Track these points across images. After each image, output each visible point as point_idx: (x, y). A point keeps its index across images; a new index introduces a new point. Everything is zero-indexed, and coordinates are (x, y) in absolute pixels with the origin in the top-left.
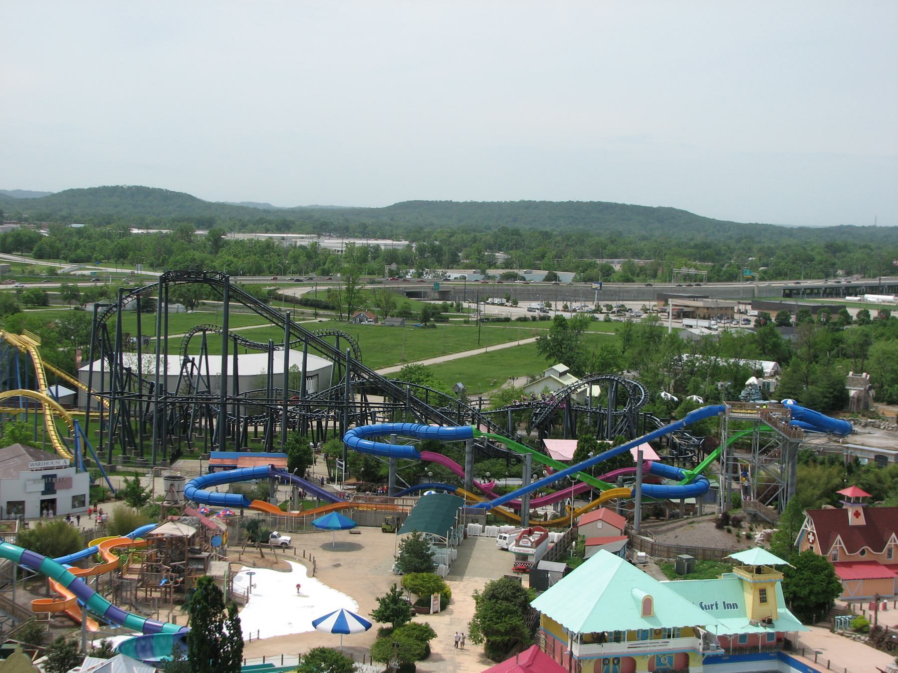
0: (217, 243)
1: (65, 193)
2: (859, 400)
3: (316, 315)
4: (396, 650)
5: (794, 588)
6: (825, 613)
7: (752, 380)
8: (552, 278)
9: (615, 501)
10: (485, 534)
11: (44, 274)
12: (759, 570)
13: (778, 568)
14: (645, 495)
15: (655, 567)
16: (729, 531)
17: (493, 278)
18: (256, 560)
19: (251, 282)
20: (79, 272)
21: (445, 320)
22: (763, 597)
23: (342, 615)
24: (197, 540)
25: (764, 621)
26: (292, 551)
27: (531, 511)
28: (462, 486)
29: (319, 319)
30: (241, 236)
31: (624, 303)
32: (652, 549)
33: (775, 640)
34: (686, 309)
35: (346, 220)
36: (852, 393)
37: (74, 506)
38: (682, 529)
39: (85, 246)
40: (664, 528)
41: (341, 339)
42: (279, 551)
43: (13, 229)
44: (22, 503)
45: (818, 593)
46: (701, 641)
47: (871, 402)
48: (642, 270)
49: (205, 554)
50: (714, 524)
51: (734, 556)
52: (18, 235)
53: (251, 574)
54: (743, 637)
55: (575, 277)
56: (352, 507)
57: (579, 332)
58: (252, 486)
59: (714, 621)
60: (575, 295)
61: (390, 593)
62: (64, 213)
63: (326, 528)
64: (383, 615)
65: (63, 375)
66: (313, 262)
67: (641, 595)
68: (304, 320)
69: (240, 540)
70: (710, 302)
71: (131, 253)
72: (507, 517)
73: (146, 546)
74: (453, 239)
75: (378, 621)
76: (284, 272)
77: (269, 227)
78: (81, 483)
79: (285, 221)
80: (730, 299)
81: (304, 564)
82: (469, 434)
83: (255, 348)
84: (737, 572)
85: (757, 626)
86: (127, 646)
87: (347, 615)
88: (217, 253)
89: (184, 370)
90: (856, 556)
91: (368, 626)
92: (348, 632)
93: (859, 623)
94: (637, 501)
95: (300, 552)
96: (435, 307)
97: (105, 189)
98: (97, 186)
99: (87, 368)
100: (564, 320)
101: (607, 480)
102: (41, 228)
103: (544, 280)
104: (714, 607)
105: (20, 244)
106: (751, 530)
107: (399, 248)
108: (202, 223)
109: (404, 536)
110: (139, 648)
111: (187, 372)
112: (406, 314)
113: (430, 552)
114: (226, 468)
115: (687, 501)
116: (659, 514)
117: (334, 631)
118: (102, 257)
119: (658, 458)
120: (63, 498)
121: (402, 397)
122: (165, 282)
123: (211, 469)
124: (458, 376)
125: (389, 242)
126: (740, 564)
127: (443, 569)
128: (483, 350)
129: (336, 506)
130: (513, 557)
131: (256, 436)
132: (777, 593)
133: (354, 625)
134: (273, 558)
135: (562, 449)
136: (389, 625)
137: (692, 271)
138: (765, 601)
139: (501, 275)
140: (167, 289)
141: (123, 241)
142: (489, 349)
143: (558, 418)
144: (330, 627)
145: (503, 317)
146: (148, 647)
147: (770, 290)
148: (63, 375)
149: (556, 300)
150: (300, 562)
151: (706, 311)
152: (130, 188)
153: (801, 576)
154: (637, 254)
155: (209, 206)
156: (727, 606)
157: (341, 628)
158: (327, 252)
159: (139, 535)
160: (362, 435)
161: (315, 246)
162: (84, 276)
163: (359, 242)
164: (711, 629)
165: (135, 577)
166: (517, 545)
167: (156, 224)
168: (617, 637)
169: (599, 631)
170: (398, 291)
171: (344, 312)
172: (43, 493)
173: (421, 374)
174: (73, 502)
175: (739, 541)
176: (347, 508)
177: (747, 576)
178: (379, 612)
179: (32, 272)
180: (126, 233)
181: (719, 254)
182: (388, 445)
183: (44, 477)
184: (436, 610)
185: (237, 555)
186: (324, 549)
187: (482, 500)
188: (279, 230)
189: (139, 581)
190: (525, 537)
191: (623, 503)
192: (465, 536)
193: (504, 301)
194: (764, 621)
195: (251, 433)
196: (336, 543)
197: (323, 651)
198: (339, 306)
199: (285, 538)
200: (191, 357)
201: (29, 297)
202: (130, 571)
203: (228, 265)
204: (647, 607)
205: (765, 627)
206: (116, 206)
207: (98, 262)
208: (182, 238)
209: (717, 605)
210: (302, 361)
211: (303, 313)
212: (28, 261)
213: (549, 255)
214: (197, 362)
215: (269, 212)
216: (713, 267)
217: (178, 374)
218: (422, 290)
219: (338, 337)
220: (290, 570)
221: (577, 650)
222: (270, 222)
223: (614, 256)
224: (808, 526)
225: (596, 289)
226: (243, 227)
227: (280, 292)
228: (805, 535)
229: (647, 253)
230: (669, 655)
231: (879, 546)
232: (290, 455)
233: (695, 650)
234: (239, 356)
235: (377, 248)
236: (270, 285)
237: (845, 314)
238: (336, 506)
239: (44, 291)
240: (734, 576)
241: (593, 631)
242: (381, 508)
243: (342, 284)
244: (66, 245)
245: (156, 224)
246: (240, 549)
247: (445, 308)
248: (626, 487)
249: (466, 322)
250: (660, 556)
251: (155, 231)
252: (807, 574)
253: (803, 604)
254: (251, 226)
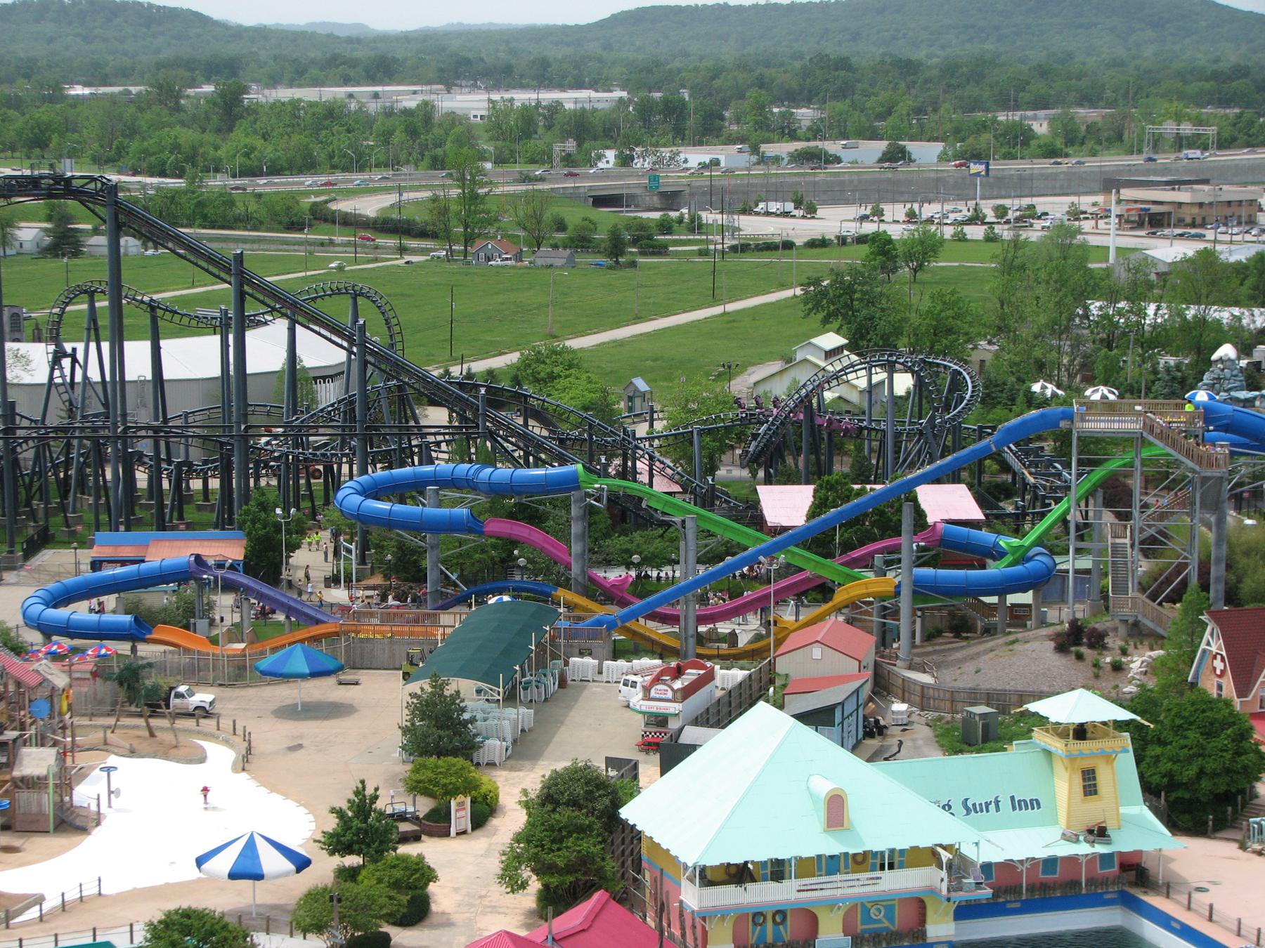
0: (230, 109)
3: (402, 250)
4: (338, 908)
5: (1169, 765)
6: (1235, 812)
7: (1227, 351)
8: (896, 155)
9: (870, 603)
10: (604, 677)
12: (1081, 732)
13: (1120, 726)
14: (921, 591)
15: (927, 732)
16: (1080, 657)
17: (777, 160)
21: (661, 250)
22: (1090, 785)
23: (250, 845)
25: (1090, 832)
26: (213, 722)
27: (702, 629)
28: (567, 585)
29: (407, 258)
31: (1035, 200)
32: (923, 697)
33: (1116, 869)
34: (1155, 209)
35: (513, 52)
38: (991, 655)
40: (959, 655)
41: (360, 300)
42: (190, 723)
45: (1215, 774)
46: (944, 874)
48: (1092, 129)
50: (1052, 644)
51: (1033, 707)
53: (109, 770)
54: (1051, 863)
55: (944, 153)
56: (346, 633)
57: (921, 266)
58: (160, 598)
59: (974, 835)
60: (933, 189)
61: (353, 797)
64: (339, 842)
66: (422, 139)
67: (823, 787)
68: (376, 260)
69: (115, 703)
70: (1204, 193)
71: (55, 138)
72: (653, 642)
74: (717, 83)
75: (332, 853)
76: (359, 163)
77: (352, 73)
79: (381, 60)
80: (1253, 183)
82: (571, 483)
83: (193, 325)
84: (1041, 738)
85: (1077, 841)
87: (260, 843)
88: (230, 130)
89: (57, 373)
91: (302, 863)
92: (259, 877)
94: (905, 603)
95: (226, 723)
96: (642, 226)
100: (890, 241)
101: (852, 564)
103: (880, 161)
104: (992, 807)
106: (1124, 652)
107: (599, 106)
108: (212, 70)
109: (415, 687)
111: (63, 376)
112: (582, 242)
113: (466, 716)
114: (123, 563)
115: (1013, 599)
116: (961, 628)
117: (233, 876)
119: (976, 513)
121: (480, 407)
123: (96, 565)
124: (649, 363)
125: (584, 94)
126: (1041, 721)
127: (494, 747)
128: (718, 310)
130: (640, 721)
131: (206, 499)
132: (1122, 772)
133: (272, 862)
135: (787, 505)
136: (353, 860)
137: (1187, 129)
138: (1096, 793)
139: (791, 155)
141: (43, 114)
142: (731, 307)
143: (800, 440)
144: (226, 870)
145: (777, 240)
149: (894, 201)
150: (226, 742)
151: (1196, 210)
153: (1182, 742)
154: (1088, 100)
155: (237, 33)
156: (1018, 804)
157: (246, 871)
158: (453, 119)
161: (426, 110)
163: (522, 97)
164: (968, 851)
166: (647, 697)
167: (125, 76)
168: (777, 870)
169: (739, 860)
170: (573, 197)
171: (457, 243)
173: (556, 363)
175: (1097, 676)
176: (337, 634)
177: (1056, 745)
178: (331, 836)
180: (56, 96)
182: (427, 509)
184: (462, 828)
185: (100, 735)
186: (351, 706)
187: (603, 612)
188: (371, 79)
190: (664, 682)
191: (885, 608)
192: (563, 683)
193: (789, 206)
194: (1090, 832)
196: (304, 704)
197: (187, 914)
198: (447, 231)
199: (202, 697)
200: (68, 347)
203: (247, 155)
204: (835, 811)
205: (1092, 843)
206: (51, 40)
209: (997, 802)
213: (903, 108)
216: (1239, 116)
217: (45, 380)
218: (624, 192)
220: (202, 760)
221: (692, 897)
222: (353, 64)
223: (1041, 103)
224: (1213, 642)
225: (978, 174)
226: (299, 74)
227: (334, 206)
228: (1208, 658)
229: (1109, 94)
230: (886, 903)
232: (249, 534)
233: (933, 891)
235: (555, 107)
240: (1037, 746)
241: (725, 860)
243: (450, 187)
245: (124, 75)
246: (111, 721)
247: (665, 227)
248: (890, 575)
249: (703, 253)
250: (936, 709)
251: (116, 89)
252: (1193, 735)
253: (1187, 796)
254: (314, 71)
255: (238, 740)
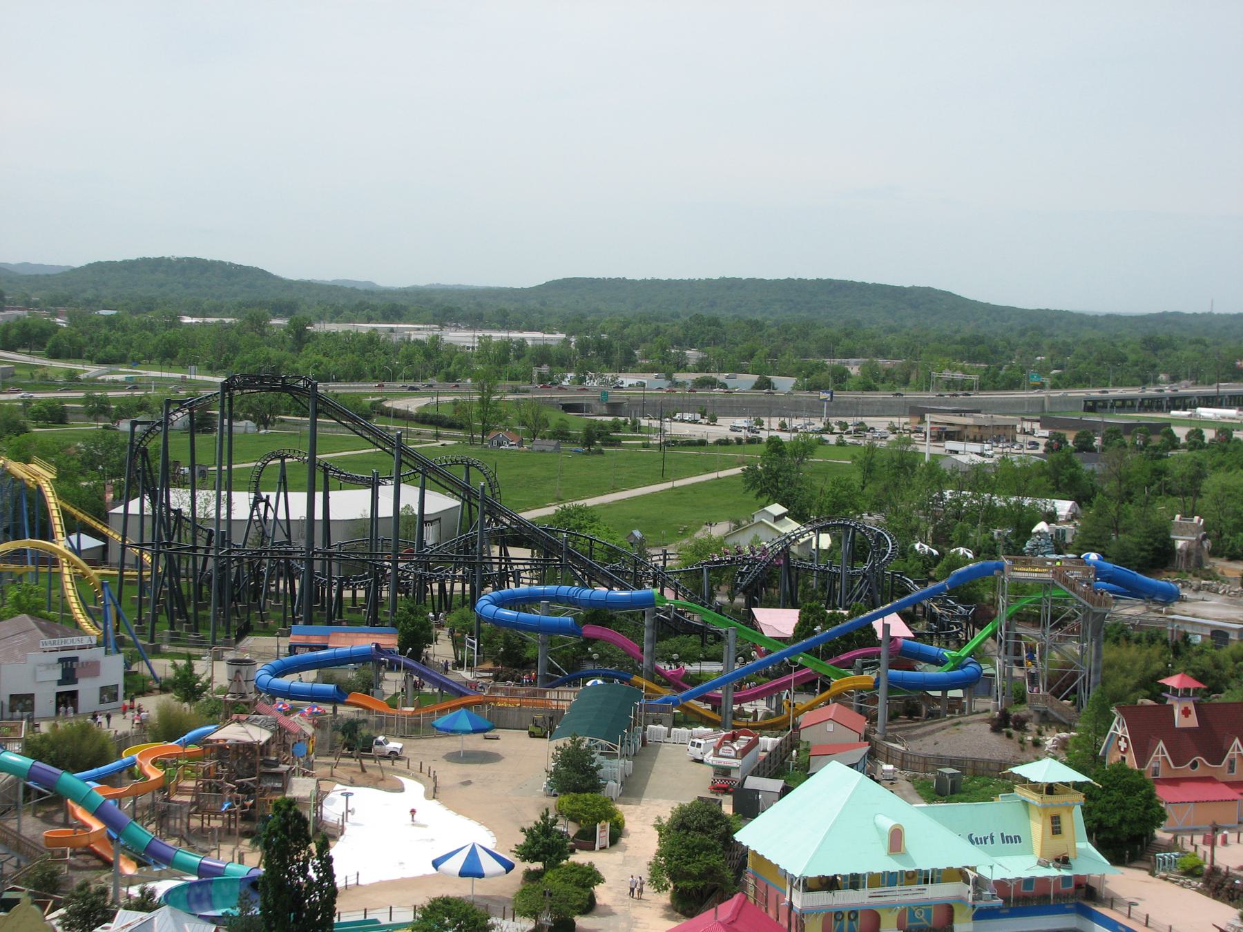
0: (300, 337)
1: (90, 267)
2: (1188, 554)
3: (438, 436)
4: (548, 901)
5: (1099, 814)
6: (1142, 849)
7: (1042, 526)
8: (764, 384)
9: (851, 694)
10: (671, 740)
11: (61, 380)
12: (1051, 789)
13: (1077, 786)
14: (893, 686)
15: (907, 785)
16: (1009, 736)
17: (683, 384)
18: (354, 776)
19: (348, 391)
20: (110, 377)
21: (616, 443)
22: (1056, 827)
23: (473, 852)
24: (273, 747)
25: (1057, 860)
26: (405, 763)
27: (735, 707)
28: (639, 673)
29: (442, 442)
30: (333, 327)
31: (864, 419)
32: (902, 760)
33: (1073, 886)
34: (949, 428)
35: (479, 304)
36: (1180, 544)
37: (102, 701)
38: (944, 732)
39: (118, 341)
40: (919, 731)
41: (472, 470)
42: (387, 763)
43: (18, 318)
44: (31, 697)
45: (1132, 822)
46: (970, 888)
47: (1205, 557)
48: (889, 373)
49: (283, 768)
50: (989, 726)
51: (1016, 770)
52: (25, 325)
53: (347, 795)
54: (1029, 882)
55: (796, 384)
56: (487, 702)
57: (801, 460)
58: (349, 674)
59: (989, 860)
60: (795, 409)
61: (539, 821)
62: (89, 295)
63: (451, 732)
64: (530, 852)
65: (87, 519)
66: (434, 363)
67: (888, 824)
68: (421, 442)
69: (333, 747)
70: (982, 419)
71: (181, 351)
72: (702, 716)
73: (201, 757)
74: (627, 331)
75: (524, 860)
76: (392, 376)
77: (373, 314)
78: (113, 669)
79: (394, 306)
80: (1010, 414)
81: (421, 781)
82: (649, 602)
83: (353, 482)
84: (1021, 792)
85: (1048, 867)
86: (176, 894)
87: (480, 852)
88: (300, 350)
89: (255, 513)
90: (1186, 770)
91: (509, 867)
92: (481, 876)
93: (1189, 863)
94: (882, 693)
95: (415, 764)
96: (602, 426)
97: (145, 262)
98: (134, 258)
99: (120, 510)
100: (781, 443)
101: (840, 664)
102: (57, 316)
103: (753, 388)
104: (989, 840)
105: (28, 338)
106: (1040, 733)
107: (553, 343)
108: (280, 309)
109: (560, 742)
110: (192, 897)
111: (259, 515)
112: (562, 435)
113: (595, 765)
114: (312, 648)
115: (951, 693)
116: (912, 712)
117: (462, 874)
118: (141, 355)
119: (910, 634)
120: (87, 690)
121: (556, 550)
122: (228, 390)
123: (292, 649)
124: (634, 520)
125: (539, 335)
126: (1024, 781)
127: (613, 788)
128: (668, 485)
129: (465, 700)
130: (710, 772)
131: (354, 604)
132: (1075, 822)
133: (489, 865)
134: (378, 773)
135: (778, 621)
136: (538, 865)
137: (958, 376)
138: (1060, 832)
139: (693, 381)
140: (231, 400)
141: (170, 334)
142: (677, 483)
143: (773, 578)
144: (457, 868)
145: (696, 439)
146: (205, 895)
147: (1066, 402)
148: (87, 519)
149: (770, 416)
150: (415, 778)
151: (977, 430)
152: (179, 260)
153: (1109, 798)
154: (881, 352)
155: (289, 285)
156: (1006, 839)
157: (471, 870)
158: (453, 349)
159: (193, 741)
160: (501, 603)
161: (436, 341)
162: (116, 382)
163: (497, 336)
164: (985, 872)
165: (187, 799)
166: (716, 755)
167: (216, 311)
168: (854, 882)
169: (830, 873)
170: (550, 403)
171: (477, 432)
172: (60, 683)
173: (582, 518)
174: (101, 695)
175: (1022, 750)
176: (480, 703)
177: (1034, 798)
178: (524, 847)
179: (44, 377)
180: (174, 323)
181: (995, 351)
182: (537, 616)
183: (61, 660)
184: (603, 844)
185: (328, 769)
186: (449, 760)
187: (667, 693)
188: (386, 319)
189: (192, 804)
190: (726, 744)
191: (862, 697)
192: (644, 743)
193: (698, 416)
194: (1057, 860)
195: (347, 599)
196: (465, 752)
197: (446, 901)
198: (469, 424)
199: (394, 745)
200: (264, 495)
201: (40, 411)
202: (180, 790)
203: (316, 367)
204: (896, 840)
205: (1059, 868)
206: (161, 286)
207: (136, 362)
208: (252, 330)
209: (992, 837)
210: (418, 499)
211: (419, 434)
212: (39, 361)
213: (760, 353)
214: (272, 501)
215: (372, 293)
216: (987, 369)
217: (247, 517)
218: (585, 402)
219: (468, 467)
220: (402, 790)
221: (799, 900)
222: (374, 308)
223: (850, 354)
224: (1119, 729)
225: (825, 400)
226: (336, 314)
227: (388, 404)
228: (1114, 740)
229: (895, 350)
230: (926, 907)
231: (1216, 755)
232: (402, 630)
233: (961, 900)
234: (331, 493)
235: (522, 343)
236: (374, 395)
237: (1170, 434)
238: (465, 700)
239: (61, 403)
240: (1017, 798)
241: (821, 874)
242: (528, 704)
243: (474, 394)
244: (92, 339)
245: (216, 310)
246: (332, 760)
247: (616, 427)
248: (866, 674)
249: (645, 446)
250: (913, 770)
251: (214, 320)
252: (1117, 794)
253: (1112, 836)
254: (347, 313)
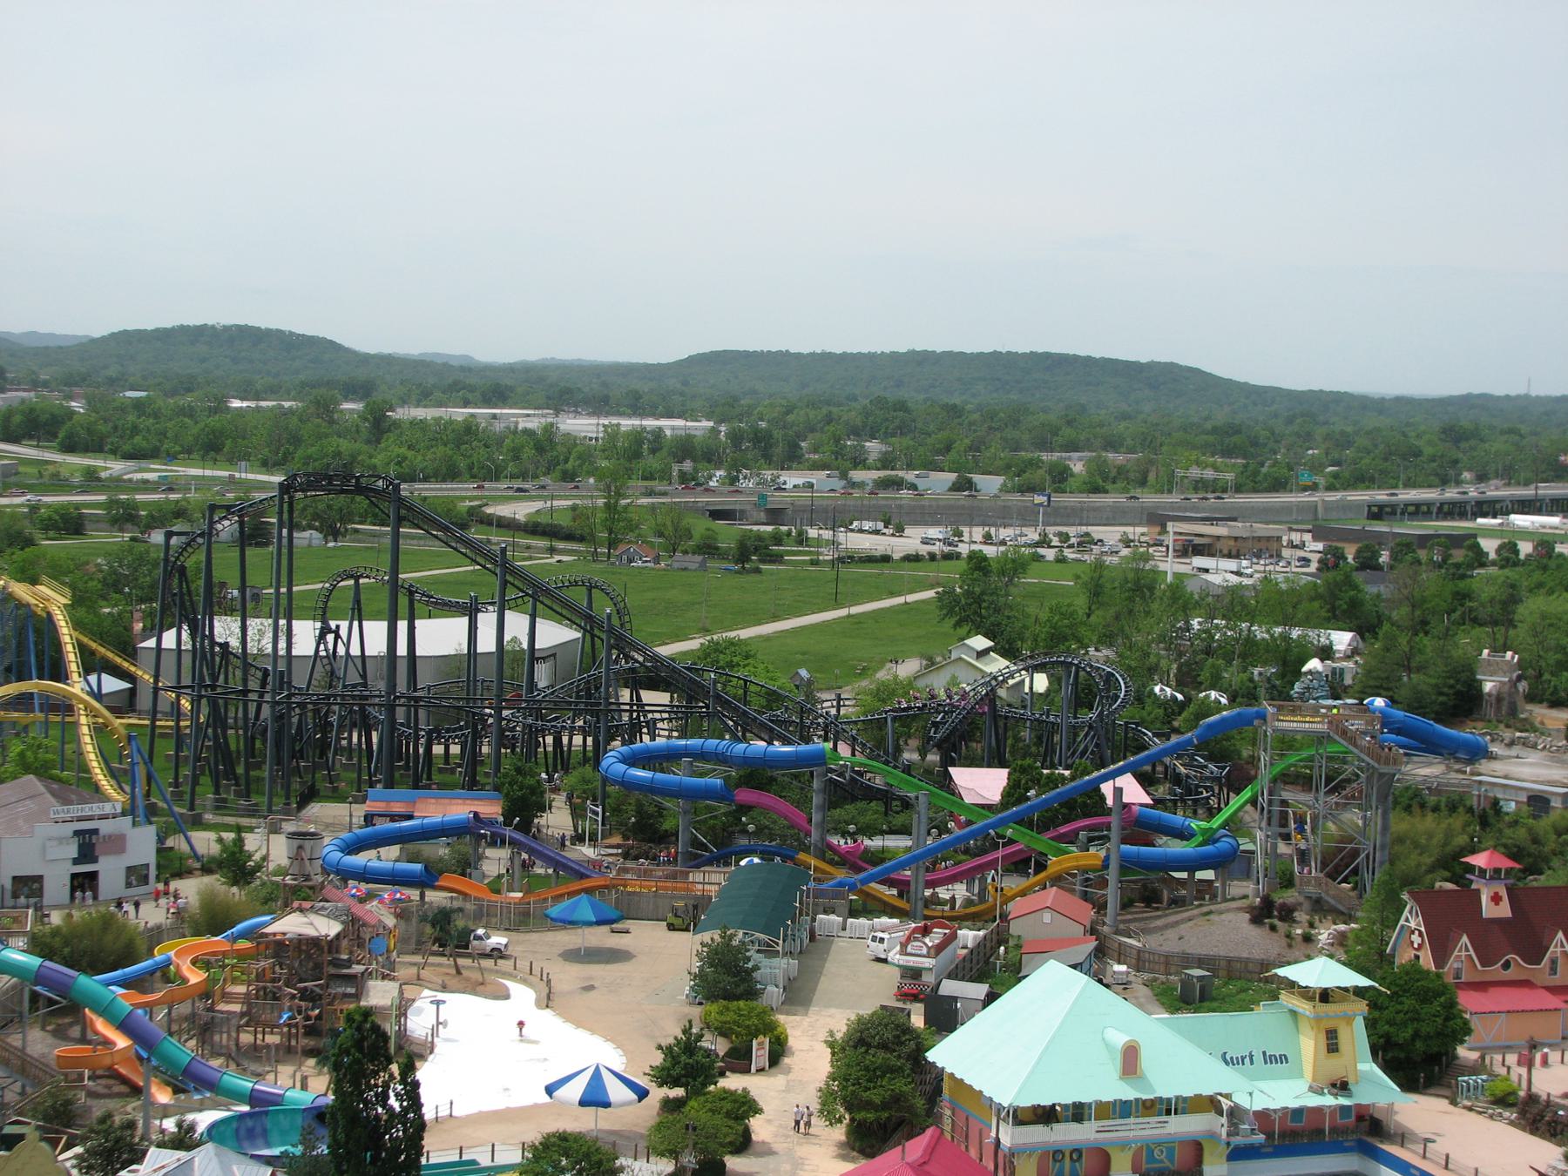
0: (379, 425)
1: (114, 336)
2: (1499, 699)
3: (552, 551)
4: (692, 1136)
5: (1386, 1027)
6: (1441, 1071)
7: (1314, 664)
8: (963, 485)
9: (1074, 876)
10: (847, 933)
11: (77, 479)
12: (1325, 996)
13: (1359, 992)
14: (1127, 865)
15: (1144, 991)
16: (1273, 928)
17: (861, 485)
18: (447, 979)
19: (439, 494)
20: (139, 476)
21: (777, 559)
22: (1332, 1043)
23: (597, 1075)
24: (345, 943)
25: (1334, 1085)
26: (510, 963)
27: (928, 893)
28: (806, 849)
29: (558, 558)
30: (420, 413)
31: (1090, 529)
32: (1138, 959)
33: (1353, 1118)
34: (1197, 541)
35: (604, 384)
36: (1488, 687)
37: (129, 885)
38: (1190, 924)
39: (149, 430)
40: (1159, 923)
41: (596, 593)
42: (488, 963)
43: (23, 401)
44: (39, 879)
45: (1428, 1037)
46: (1224, 1120)
47: (1521, 703)
48: (1121, 471)
49: (358, 969)
50: (1247, 916)
51: (1281, 972)
52: (32, 410)
53: (438, 1003)
54: (1298, 1113)
55: (1004, 485)
56: (615, 886)
57: (1011, 580)
58: (441, 850)
59: (1247, 1085)
60: (1003, 516)
61: (680, 1035)
62: (112, 372)
63: (569, 923)
64: (669, 1075)
65: (110, 655)
66: (547, 458)
67: (1120, 1039)
68: (531, 558)
69: (420, 943)
70: (1239, 528)
71: (229, 442)
72: (885, 903)
73: (254, 955)
74: (790, 418)
75: (661, 1086)
76: (495, 474)
77: (470, 396)
78: (142, 844)
79: (497, 386)
80: (1274, 523)
81: (531, 985)
82: (819, 759)
83: (446, 608)
84: (1287, 1000)
85: (1322, 1094)
86: (222, 1128)
87: (606, 1075)
88: (378, 441)
89: (322, 647)
90: (1495, 971)
91: (642, 1094)
92: (607, 1105)
93: (1500, 1088)
94: (1112, 875)
95: (523, 964)
96: (759, 537)
97: (183, 330)
98: (169, 325)
99: (151, 643)
100: (985, 559)
101: (1060, 838)
102: (72, 398)
103: (951, 489)
104: (1247, 1060)
105: (35, 426)
106: (1312, 925)
107: (697, 433)
108: (353, 390)
109: (706, 937)
110: (242, 1132)
111: (326, 650)
112: (708, 549)
113: (750, 965)
114: (394, 818)
115: (1200, 875)
116: (1150, 898)
117: (583, 1103)
118: (178, 448)
119: (1148, 800)
120: (110, 870)
121: (702, 694)
122: (288, 492)
123: (369, 819)
124: (799, 657)
125: (679, 423)
126: (1291, 985)
127: (773, 994)
128: (843, 612)
129: (586, 884)
130: (896, 974)
131: (447, 762)
132: (1356, 1037)
133: (617, 1092)
134: (476, 976)
135: (982, 784)
136: (679, 1092)
137: (1209, 474)
138: (1337, 1050)
139: (875, 481)
140: (291, 504)
141: (214, 421)
142: (855, 610)
143: (975, 730)
144: (577, 1096)
145: (878, 554)
146: (258, 1130)
147: (1345, 507)
148: (110, 655)
149: (971, 525)
150: (524, 981)
151: (1232, 543)
152: (226, 329)
153: (1399, 1007)
154: (1112, 444)
155: (365, 359)
156: (1269, 1059)
157: (595, 1098)
158: (571, 441)
159: (243, 935)
160: (632, 760)
161: (549, 430)
162: (146, 482)
163: (627, 423)
164: (1242, 1100)
165: (236, 1008)
166: (903, 952)
167: (273, 392)
168: (1078, 1112)
169: (1047, 1102)
170: (694, 509)
171: (601, 546)
172: (76, 862)
173: (734, 654)
174: (128, 877)
175: (1290, 946)
176: (606, 887)
177: (1304, 1007)
178: (662, 1069)
179: (56, 475)
180: (220, 407)
181: (1255, 443)
182: (678, 777)
183: (77, 833)
184: (761, 1065)
185: (414, 970)
186: (566, 959)
187: (841, 875)
188: (487, 402)
189: (243, 1014)
190: (916, 939)
191: (1087, 880)
192: (812, 937)
193: (880, 525)
194: (1334, 1085)
195: (438, 756)
196: (586, 949)
197: (563, 1137)
198: (592, 535)
199: (497, 940)
200: (333, 624)
201: (50, 519)
202: (227, 997)
203: (399, 463)
204: (1130, 1060)
205: (1335, 1095)
206: (203, 360)
207: (172, 457)
208: (318, 416)
209: (1251, 1056)
210: (527, 630)
211: (528, 547)
212: (49, 456)
213: (959, 446)
214: (344, 633)
215: (470, 370)
216: (1245, 466)
217: (312, 653)
218: (738, 507)
219: (590, 589)
220: (507, 997)
221: (1008, 1136)
222: (472, 389)
223: (1072, 447)
224: (1412, 920)
225: (1041, 505)
226: (424, 397)
227: (489, 510)
228: (1406, 934)
229: (1129, 442)
230: (1168, 1144)
231: (1534, 953)
232: (507, 795)
233: (1213, 1136)
234: (417, 622)
235: (658, 433)
236: (471, 499)
237: (1476, 548)
238: (586, 884)
239: (77, 508)
240: (1282, 1006)
241: (1036, 1103)
242: (666, 888)
243: (597, 497)
244: (115, 428)
245: (272, 391)
246: (418, 959)
247: (778, 539)
248: (1092, 850)
249: (814, 563)
250: (1152, 971)
251: (270, 404)
252: (1409, 1002)
253: (1402, 1055)
254: (438, 394)
255: (544, 984)
